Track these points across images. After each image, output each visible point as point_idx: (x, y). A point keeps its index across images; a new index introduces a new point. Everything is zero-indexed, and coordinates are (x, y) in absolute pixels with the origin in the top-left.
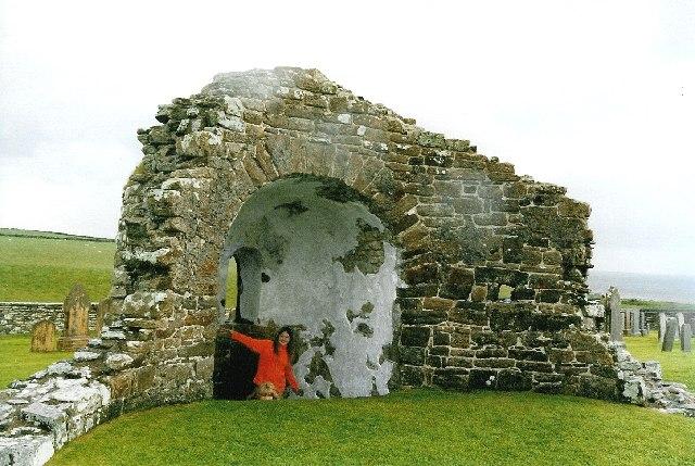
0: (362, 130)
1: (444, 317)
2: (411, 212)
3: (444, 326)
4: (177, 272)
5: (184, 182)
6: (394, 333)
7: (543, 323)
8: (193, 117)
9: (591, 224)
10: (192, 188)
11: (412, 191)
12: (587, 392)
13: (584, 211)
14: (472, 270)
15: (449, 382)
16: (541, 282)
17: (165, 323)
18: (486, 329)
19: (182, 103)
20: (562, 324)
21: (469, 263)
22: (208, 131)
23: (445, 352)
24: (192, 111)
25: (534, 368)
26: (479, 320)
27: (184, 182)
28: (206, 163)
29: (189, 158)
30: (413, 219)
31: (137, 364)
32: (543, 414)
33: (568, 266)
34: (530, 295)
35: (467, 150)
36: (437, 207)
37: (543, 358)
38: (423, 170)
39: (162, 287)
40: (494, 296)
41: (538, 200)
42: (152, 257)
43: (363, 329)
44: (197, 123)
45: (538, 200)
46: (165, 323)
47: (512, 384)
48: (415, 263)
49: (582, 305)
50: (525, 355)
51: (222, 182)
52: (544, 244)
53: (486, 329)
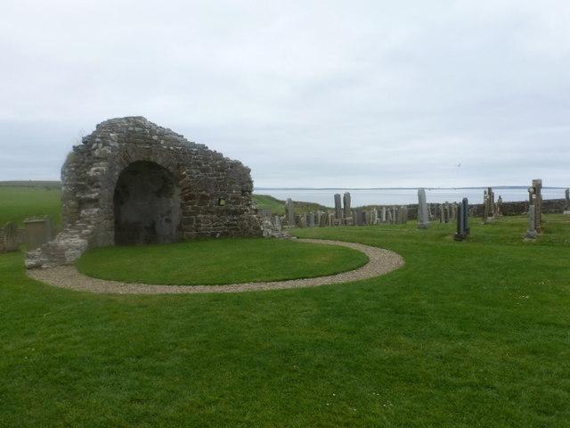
0: (162, 142)
3: (199, 216)
7: (235, 213)
12: (251, 236)
13: (249, 170)
14: (208, 194)
20: (242, 212)
22: (105, 148)
24: (98, 140)
26: (212, 213)
29: (98, 158)
30: (185, 176)
42: (93, 196)
47: (225, 235)
50: (229, 225)
51: (111, 168)
52: (234, 183)
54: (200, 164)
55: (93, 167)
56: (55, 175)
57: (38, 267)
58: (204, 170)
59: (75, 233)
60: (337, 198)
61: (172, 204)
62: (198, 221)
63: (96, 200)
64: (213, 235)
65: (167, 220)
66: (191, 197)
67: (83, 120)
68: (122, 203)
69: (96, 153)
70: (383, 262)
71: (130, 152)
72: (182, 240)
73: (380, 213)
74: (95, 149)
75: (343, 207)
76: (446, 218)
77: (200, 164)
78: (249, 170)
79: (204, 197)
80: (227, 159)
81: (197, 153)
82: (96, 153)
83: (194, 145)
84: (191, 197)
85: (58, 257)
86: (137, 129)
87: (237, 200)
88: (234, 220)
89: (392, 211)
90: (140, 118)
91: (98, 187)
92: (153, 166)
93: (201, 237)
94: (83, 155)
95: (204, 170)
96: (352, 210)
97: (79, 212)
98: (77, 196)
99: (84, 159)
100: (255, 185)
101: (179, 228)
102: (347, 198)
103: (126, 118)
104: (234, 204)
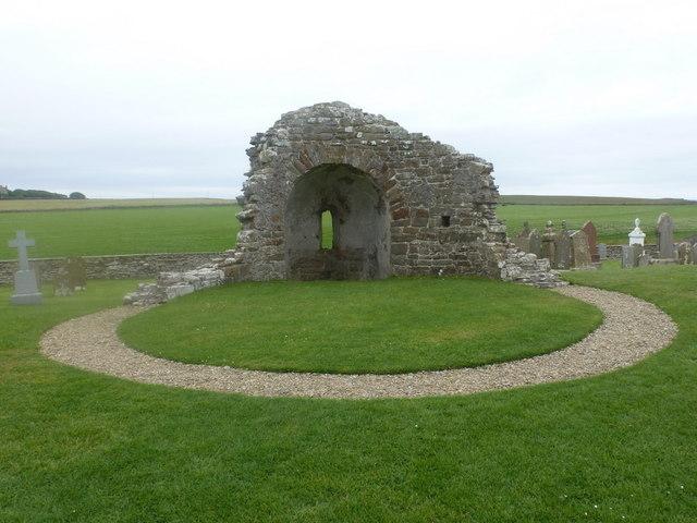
0: (360, 135)
1: (414, 238)
3: (415, 242)
4: (257, 220)
6: (373, 116)
8: (263, 142)
10: (261, 179)
11: (392, 166)
15: (416, 272)
16: (461, 215)
19: (260, 135)
20: (473, 238)
21: (425, 205)
23: (416, 257)
24: (263, 139)
30: (394, 183)
31: (238, 262)
35: (421, 139)
36: (407, 175)
37: (465, 258)
38: (397, 154)
39: (251, 228)
41: (459, 165)
44: (265, 145)
45: (459, 165)
50: (456, 257)
62: (413, 250)
68: (342, 222)
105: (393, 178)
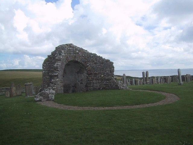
2: (88, 65)
5: (59, 64)
7: (108, 80)
8: (57, 54)
9: (114, 65)
12: (114, 89)
13: (113, 63)
17: (58, 83)
18: (100, 81)
20: (111, 80)
22: (60, 56)
25: (107, 86)
26: (99, 80)
27: (59, 64)
28: (61, 61)
30: (88, 66)
32: (156, 125)
33: (111, 71)
34: (105, 76)
40: (101, 76)
42: (56, 74)
43: (81, 83)
44: (58, 55)
46: (58, 83)
47: (104, 88)
48: (89, 72)
49: (113, 77)
51: (62, 63)
53: (100, 81)
54: (94, 61)
55: (56, 63)
56: (51, 54)
57: (40, 101)
58: (95, 63)
59: (51, 88)
60: (143, 73)
61: (83, 77)
62: (93, 83)
63: (57, 76)
64: (99, 89)
65: (81, 83)
66: (91, 74)
67: (49, 48)
69: (57, 58)
70: (171, 99)
71: (68, 57)
72: (87, 91)
73: (157, 79)
74: (56, 56)
75: (145, 77)
76: (187, 81)
77: (94, 61)
78: (113, 63)
79: (96, 74)
80: (104, 59)
81: (93, 57)
82: (57, 58)
83: (91, 54)
84: (91, 74)
85: (48, 99)
86: (71, 48)
87: (108, 75)
88: (107, 83)
89: (162, 79)
90: (71, 44)
91: (58, 71)
92: (77, 62)
93: (95, 89)
94: (51, 60)
95: (95, 63)
96: (149, 78)
97: (51, 80)
98: (50, 74)
99: (52, 60)
100: (115, 69)
101: (86, 86)
102: (147, 73)
103: (66, 44)
104: (107, 76)
105: (88, 65)
